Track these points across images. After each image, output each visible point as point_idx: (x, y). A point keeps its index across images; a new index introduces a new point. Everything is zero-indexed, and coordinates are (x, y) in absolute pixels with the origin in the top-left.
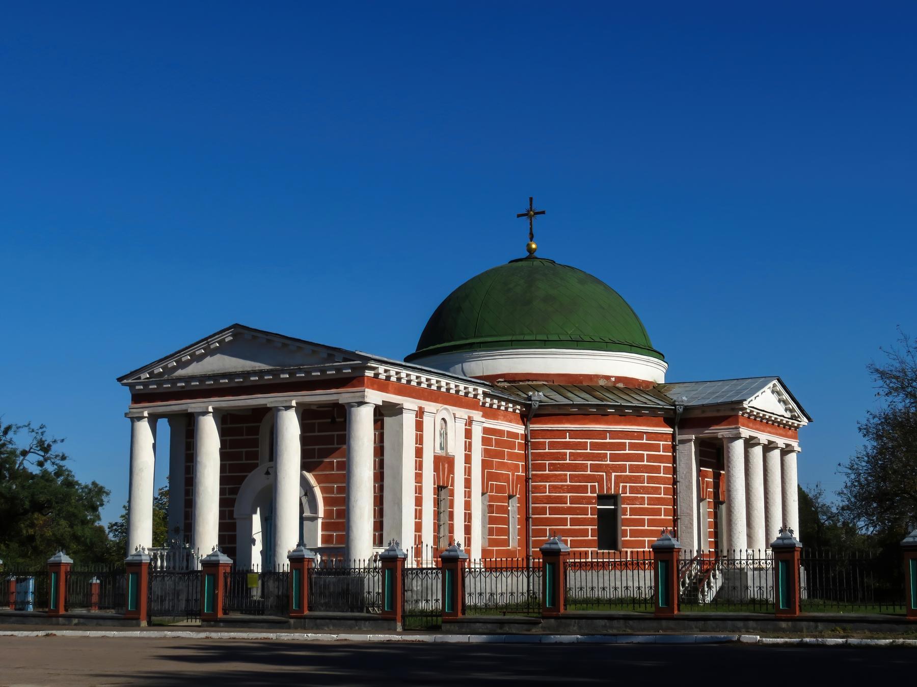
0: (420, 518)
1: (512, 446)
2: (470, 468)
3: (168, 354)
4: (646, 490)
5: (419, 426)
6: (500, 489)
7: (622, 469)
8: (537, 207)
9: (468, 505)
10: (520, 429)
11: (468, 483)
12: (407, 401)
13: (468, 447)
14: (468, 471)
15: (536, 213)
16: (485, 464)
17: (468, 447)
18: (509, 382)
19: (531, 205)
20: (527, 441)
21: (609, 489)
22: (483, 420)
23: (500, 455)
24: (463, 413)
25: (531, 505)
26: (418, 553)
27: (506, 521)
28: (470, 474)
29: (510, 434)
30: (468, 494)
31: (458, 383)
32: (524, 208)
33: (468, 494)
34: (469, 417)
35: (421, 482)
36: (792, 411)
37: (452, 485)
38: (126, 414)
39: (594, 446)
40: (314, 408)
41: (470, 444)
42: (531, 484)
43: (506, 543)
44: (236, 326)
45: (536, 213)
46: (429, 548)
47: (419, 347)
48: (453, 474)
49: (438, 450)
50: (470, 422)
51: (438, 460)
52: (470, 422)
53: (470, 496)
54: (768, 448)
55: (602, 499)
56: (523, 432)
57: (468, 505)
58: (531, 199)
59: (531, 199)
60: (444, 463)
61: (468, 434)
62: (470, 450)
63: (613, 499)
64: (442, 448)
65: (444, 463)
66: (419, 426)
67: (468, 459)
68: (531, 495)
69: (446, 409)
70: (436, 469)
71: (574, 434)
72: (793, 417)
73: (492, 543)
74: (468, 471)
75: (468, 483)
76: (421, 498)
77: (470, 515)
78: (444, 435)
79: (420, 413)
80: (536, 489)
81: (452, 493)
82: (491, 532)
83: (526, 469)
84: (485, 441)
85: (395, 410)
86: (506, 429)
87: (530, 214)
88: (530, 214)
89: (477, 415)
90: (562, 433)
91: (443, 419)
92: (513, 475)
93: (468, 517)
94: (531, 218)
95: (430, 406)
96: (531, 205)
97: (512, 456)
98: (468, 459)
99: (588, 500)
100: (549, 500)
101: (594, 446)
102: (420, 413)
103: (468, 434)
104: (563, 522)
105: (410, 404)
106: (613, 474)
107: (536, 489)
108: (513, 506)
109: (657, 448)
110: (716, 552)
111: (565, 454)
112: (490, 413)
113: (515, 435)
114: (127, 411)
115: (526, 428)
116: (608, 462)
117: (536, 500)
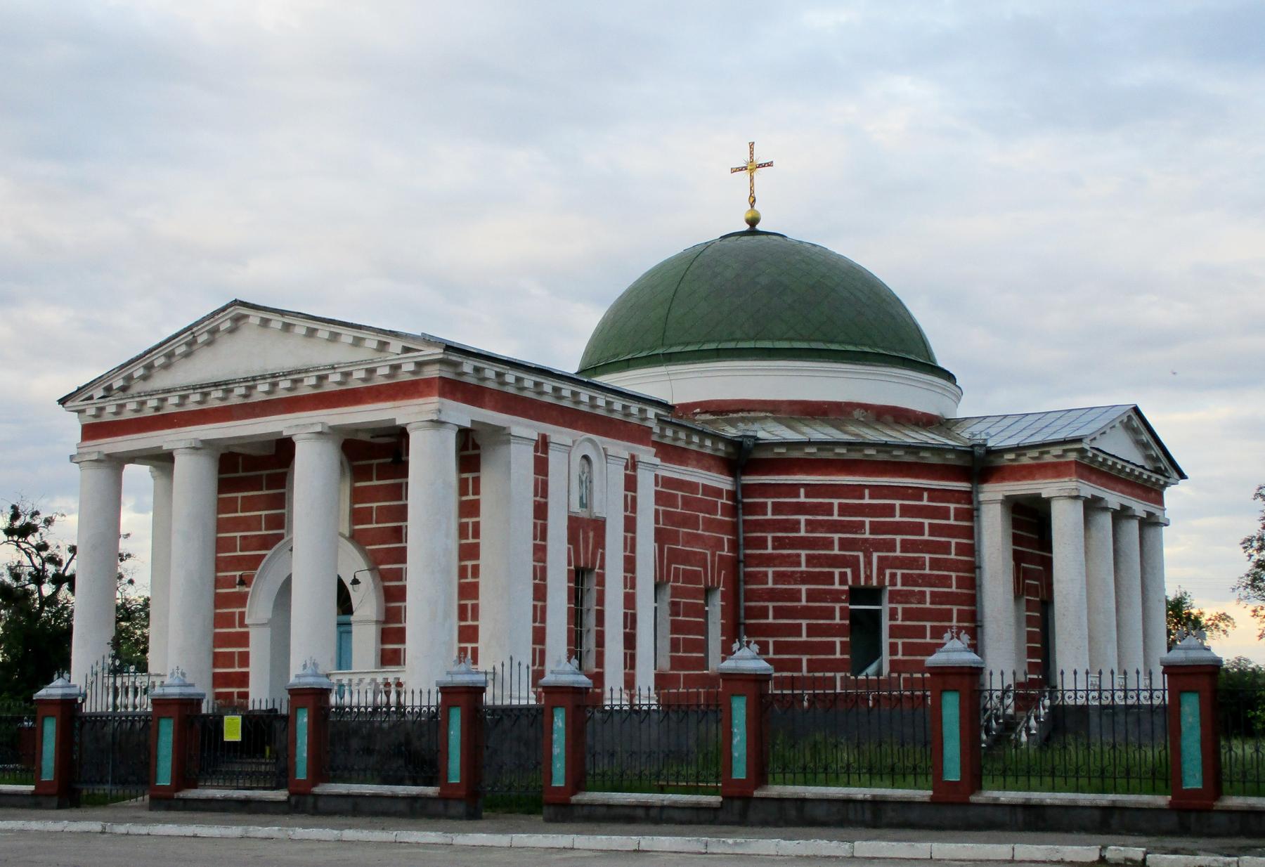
0: (543, 620)
1: (712, 508)
2: (634, 540)
3: (133, 356)
4: (928, 581)
5: (541, 466)
6: (691, 577)
7: (890, 546)
8: (760, 158)
9: (630, 601)
10: (723, 482)
11: (630, 564)
12: (519, 424)
13: (631, 505)
14: (630, 545)
15: (761, 166)
16: (661, 536)
17: (631, 505)
18: (713, 413)
19: (752, 153)
20: (738, 502)
21: (868, 577)
22: (657, 461)
23: (691, 522)
24: (621, 449)
25: (743, 604)
26: (630, 683)
27: (703, 629)
28: (633, 550)
29: (707, 490)
30: (630, 582)
31: (611, 398)
32: (743, 159)
33: (630, 582)
34: (633, 457)
35: (544, 561)
36: (1157, 459)
37: (602, 567)
38: (72, 457)
39: (844, 510)
40: (365, 437)
41: (634, 499)
42: (743, 569)
43: (703, 663)
44: (237, 303)
45: (761, 166)
46: (524, 668)
47: (582, 372)
48: (603, 548)
49: (576, 507)
50: (633, 464)
51: (575, 525)
52: (633, 464)
53: (633, 586)
54: (1121, 515)
55: (856, 594)
56: (729, 487)
57: (630, 601)
58: (752, 145)
59: (752, 145)
60: (586, 531)
61: (631, 483)
62: (634, 509)
63: (873, 595)
64: (583, 505)
65: (586, 531)
66: (541, 466)
67: (630, 525)
68: (743, 587)
69: (590, 440)
70: (573, 539)
71: (812, 490)
72: (1157, 471)
73: (676, 663)
74: (630, 545)
75: (630, 564)
76: (545, 586)
77: (634, 617)
78: (586, 483)
79: (543, 444)
80: (752, 578)
81: (601, 581)
82: (675, 645)
83: (734, 546)
84: (660, 498)
85: (500, 435)
86: (701, 481)
87: (752, 167)
88: (752, 167)
89: (646, 454)
90: (793, 489)
91: (586, 457)
92: (713, 555)
93: (630, 621)
94: (752, 171)
95: (560, 435)
96: (752, 153)
97: (709, 524)
98: (630, 525)
99: (835, 596)
100: (772, 595)
101: (844, 510)
102: (543, 444)
103: (631, 483)
104: (796, 630)
105: (524, 429)
106: (875, 556)
107: (752, 578)
108: (716, 607)
109: (944, 514)
110: (739, 798)
111: (798, 522)
112: (668, 453)
113: (718, 492)
114: (75, 453)
115: (736, 482)
116: (867, 536)
117: (751, 595)
